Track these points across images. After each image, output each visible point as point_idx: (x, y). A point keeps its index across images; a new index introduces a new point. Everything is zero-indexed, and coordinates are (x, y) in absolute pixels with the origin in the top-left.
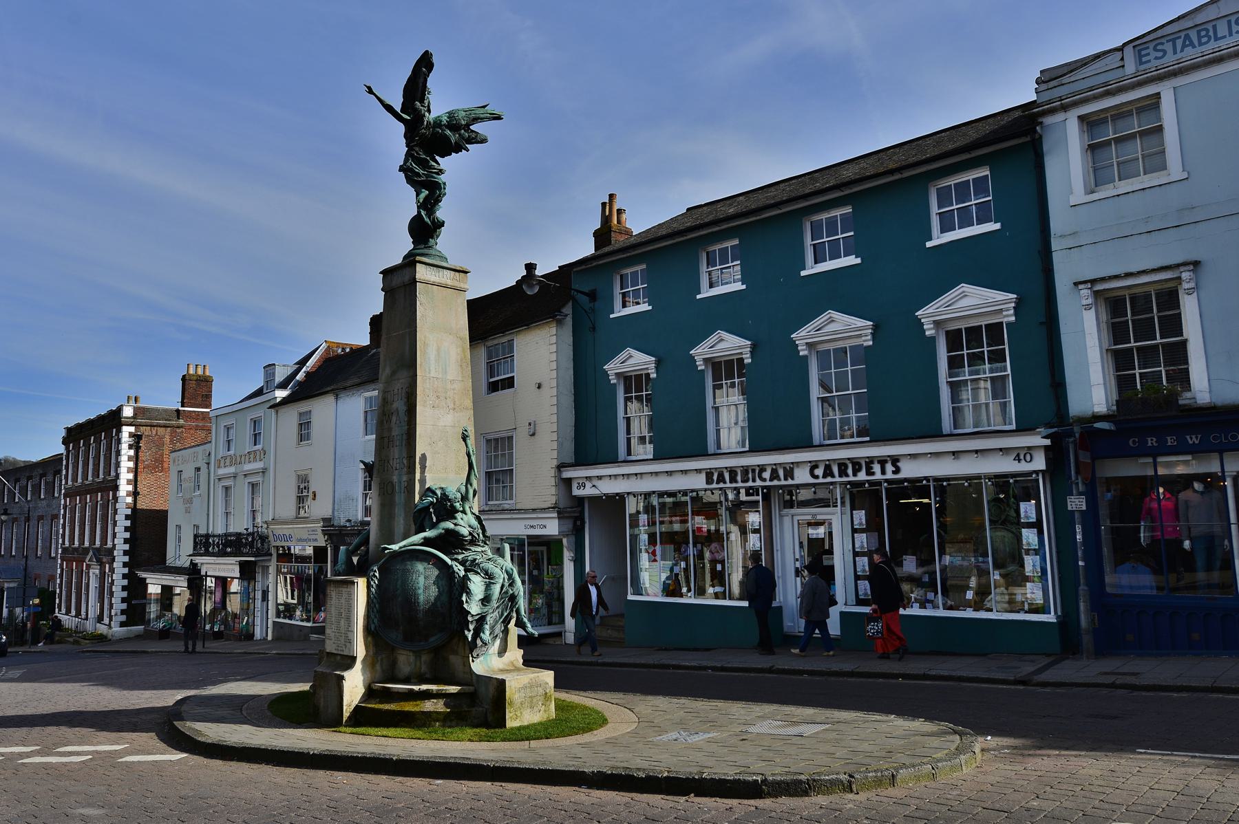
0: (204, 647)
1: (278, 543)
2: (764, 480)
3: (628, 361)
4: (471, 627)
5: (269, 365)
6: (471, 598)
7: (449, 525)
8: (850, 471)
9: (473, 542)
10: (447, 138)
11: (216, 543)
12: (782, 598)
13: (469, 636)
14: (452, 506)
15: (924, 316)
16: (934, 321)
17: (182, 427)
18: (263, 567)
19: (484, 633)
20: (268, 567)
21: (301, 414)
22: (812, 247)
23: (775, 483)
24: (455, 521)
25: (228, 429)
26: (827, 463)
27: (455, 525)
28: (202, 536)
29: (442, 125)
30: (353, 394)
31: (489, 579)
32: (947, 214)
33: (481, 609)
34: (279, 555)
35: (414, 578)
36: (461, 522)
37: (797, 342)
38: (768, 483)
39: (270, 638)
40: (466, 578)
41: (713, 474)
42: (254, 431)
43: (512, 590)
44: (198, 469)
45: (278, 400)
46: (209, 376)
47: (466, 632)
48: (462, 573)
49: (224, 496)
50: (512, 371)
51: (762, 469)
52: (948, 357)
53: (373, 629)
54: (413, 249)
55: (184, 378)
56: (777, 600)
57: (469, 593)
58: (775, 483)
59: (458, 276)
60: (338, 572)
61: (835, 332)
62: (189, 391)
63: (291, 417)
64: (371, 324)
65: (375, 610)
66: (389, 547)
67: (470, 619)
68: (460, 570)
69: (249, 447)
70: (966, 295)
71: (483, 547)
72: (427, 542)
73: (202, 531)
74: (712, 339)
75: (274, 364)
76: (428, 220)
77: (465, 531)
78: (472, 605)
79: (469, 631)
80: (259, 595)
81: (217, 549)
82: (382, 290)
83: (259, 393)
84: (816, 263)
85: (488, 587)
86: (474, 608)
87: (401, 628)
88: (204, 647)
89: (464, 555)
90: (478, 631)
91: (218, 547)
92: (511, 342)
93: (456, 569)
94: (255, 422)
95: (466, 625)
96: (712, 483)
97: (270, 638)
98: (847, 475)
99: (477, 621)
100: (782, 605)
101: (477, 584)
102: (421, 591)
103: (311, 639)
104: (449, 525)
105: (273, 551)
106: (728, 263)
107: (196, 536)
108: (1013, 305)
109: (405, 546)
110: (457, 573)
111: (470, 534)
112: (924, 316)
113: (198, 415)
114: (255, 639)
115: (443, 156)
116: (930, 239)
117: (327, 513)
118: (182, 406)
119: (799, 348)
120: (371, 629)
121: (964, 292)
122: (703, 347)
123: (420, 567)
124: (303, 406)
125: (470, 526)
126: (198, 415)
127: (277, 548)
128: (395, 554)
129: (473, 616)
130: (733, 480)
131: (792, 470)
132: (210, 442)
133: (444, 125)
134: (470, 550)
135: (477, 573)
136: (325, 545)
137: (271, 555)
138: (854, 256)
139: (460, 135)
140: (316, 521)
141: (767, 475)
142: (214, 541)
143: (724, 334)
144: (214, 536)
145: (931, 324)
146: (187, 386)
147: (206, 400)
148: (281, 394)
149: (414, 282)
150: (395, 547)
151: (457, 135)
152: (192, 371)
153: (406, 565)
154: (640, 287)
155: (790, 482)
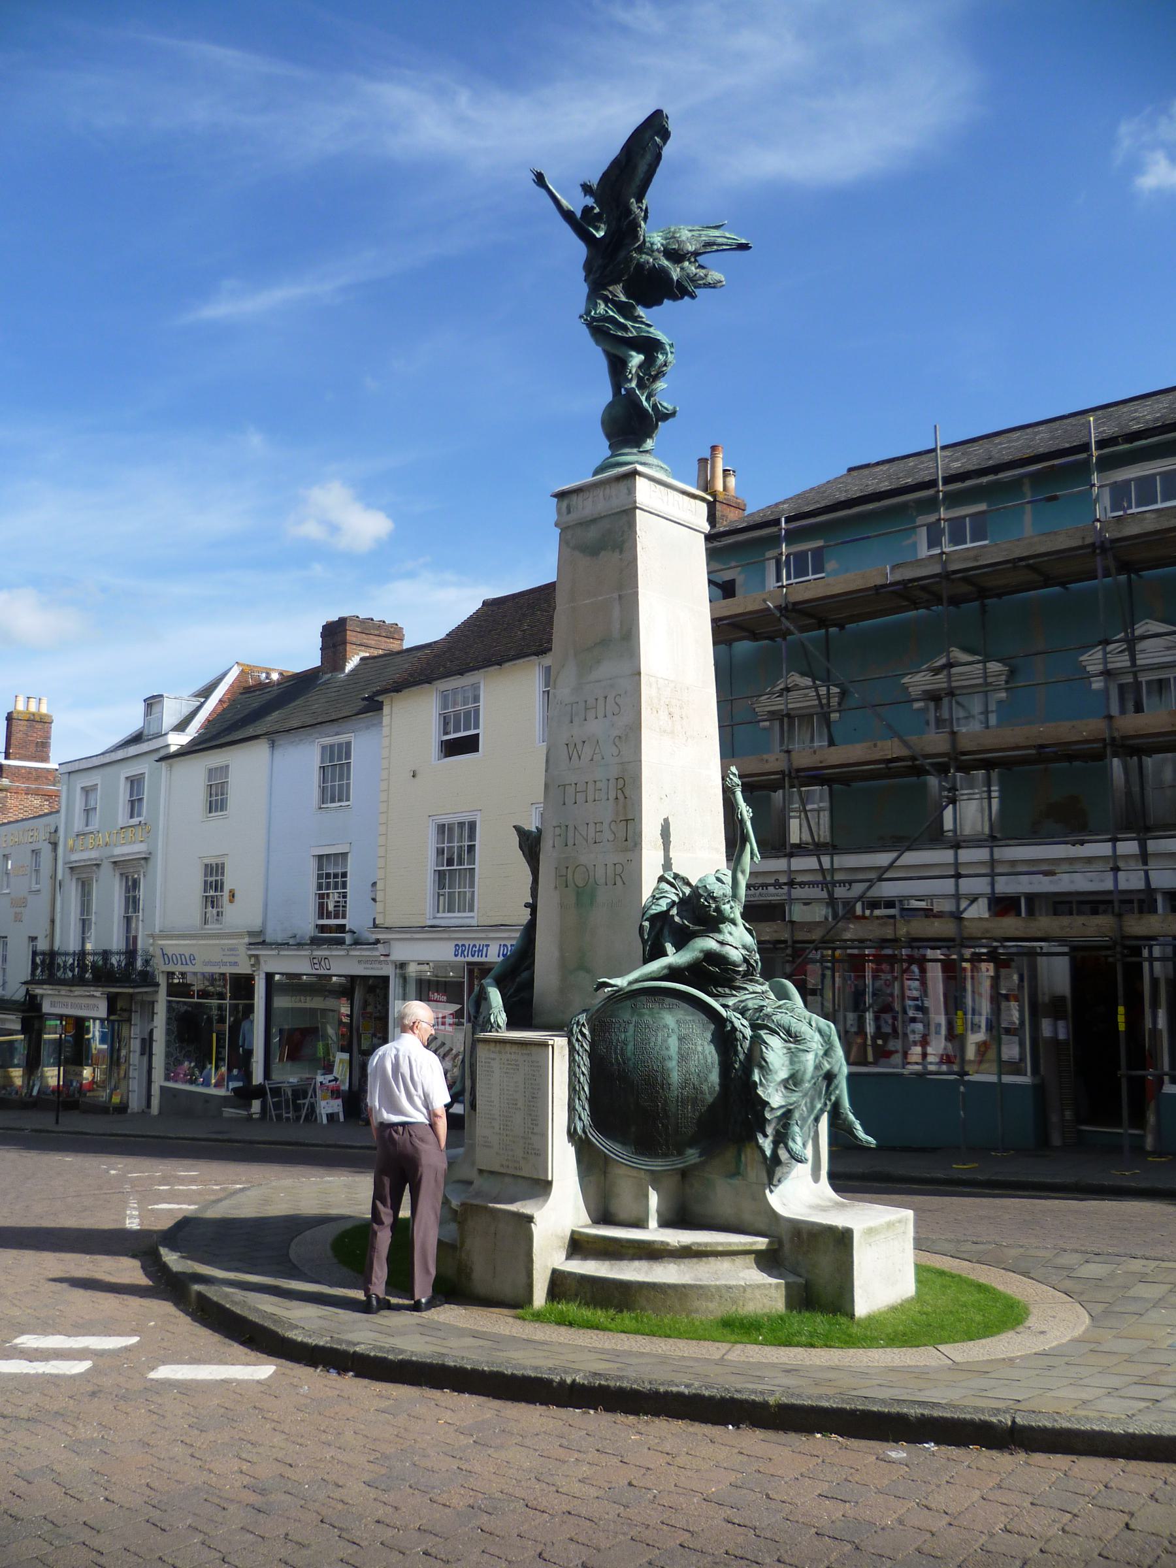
0: (57, 1122)
1: (170, 968)
4: (770, 1130)
5: (154, 697)
6: (769, 1077)
7: (710, 944)
9: (748, 975)
10: (663, 273)
11: (62, 970)
13: (767, 1144)
14: (718, 909)
15: (1091, 662)
17: (6, 790)
18: (143, 1003)
19: (794, 1140)
20: (153, 1003)
21: (211, 772)
24: (720, 937)
25: (87, 791)
27: (722, 943)
28: (43, 954)
29: (653, 251)
30: (301, 740)
31: (794, 1043)
33: (785, 1097)
34: (170, 986)
35: (660, 1039)
36: (729, 939)
39: (155, 1109)
40: (757, 1041)
42: (131, 795)
43: (829, 1063)
44: (36, 853)
45: (173, 749)
46: (46, 715)
47: (761, 1140)
48: (748, 1032)
49: (79, 895)
50: (477, 726)
53: (579, 1131)
54: (612, 456)
55: (10, 718)
57: (765, 1068)
59: (693, 505)
62: (17, 736)
63: (196, 771)
64: (323, 635)
65: (583, 1097)
66: (612, 981)
67: (768, 1116)
68: (742, 1024)
69: (122, 818)
71: (762, 984)
72: (674, 973)
73: (42, 945)
75: (161, 696)
76: (647, 405)
77: (735, 955)
78: (770, 1090)
79: (766, 1136)
80: (136, 1045)
81: (70, 974)
82: (556, 525)
83: (137, 739)
85: (793, 1056)
86: (775, 1098)
87: (633, 1129)
88: (57, 1122)
89: (738, 999)
90: (781, 1138)
91: (72, 970)
92: (476, 687)
93: (737, 1024)
94: (135, 783)
95: (760, 1124)
97: (155, 1109)
99: (779, 1118)
101: (776, 1051)
102: (672, 1064)
103: (225, 1115)
104: (710, 944)
105: (162, 980)
107: (35, 954)
109: (636, 981)
110: (741, 1032)
111: (746, 960)
112: (1091, 662)
113: (30, 773)
114: (129, 1111)
115: (648, 305)
117: (256, 924)
118: (7, 757)
120: (575, 1129)
123: (669, 1019)
124: (215, 759)
125: (744, 947)
126: (30, 773)
127: (170, 975)
128: (621, 997)
129: (772, 1109)
130: (339, 906)
132: (58, 812)
133: (658, 250)
134: (746, 989)
135: (773, 1032)
136: (249, 972)
137: (158, 985)
139: (682, 269)
140: (239, 935)
142: (65, 962)
144: (66, 954)
146: (14, 729)
147: (41, 750)
148: (176, 741)
149: (628, 513)
150: (621, 982)
151: (678, 269)
152: (21, 707)
153: (641, 1015)
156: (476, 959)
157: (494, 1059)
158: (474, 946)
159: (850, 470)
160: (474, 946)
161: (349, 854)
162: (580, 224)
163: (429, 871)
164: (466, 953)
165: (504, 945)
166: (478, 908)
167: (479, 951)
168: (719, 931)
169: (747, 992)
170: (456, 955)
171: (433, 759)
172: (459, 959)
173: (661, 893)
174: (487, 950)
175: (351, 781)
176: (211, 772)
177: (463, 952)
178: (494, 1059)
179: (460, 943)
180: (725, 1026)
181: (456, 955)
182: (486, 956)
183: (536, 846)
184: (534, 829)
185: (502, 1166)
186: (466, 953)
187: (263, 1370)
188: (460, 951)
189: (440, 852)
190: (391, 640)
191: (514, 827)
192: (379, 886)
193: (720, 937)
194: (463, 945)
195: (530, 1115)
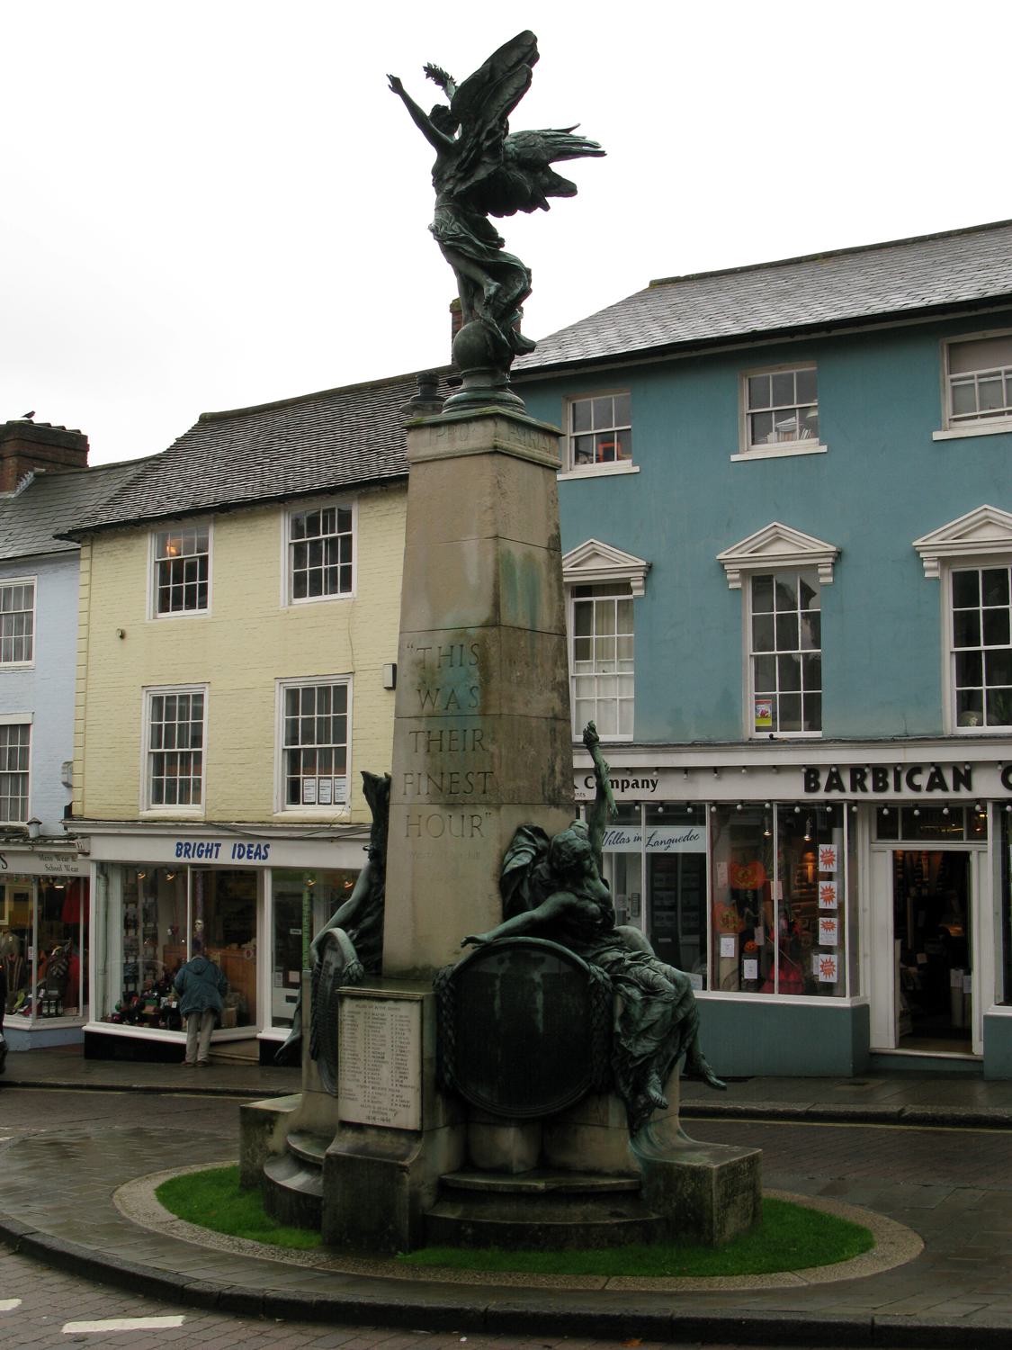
2: (917, 788)
3: (971, 535)
8: (869, 783)
12: (868, 994)
16: (939, 558)
22: (573, 441)
23: (938, 794)
24: (580, 892)
26: (834, 770)
32: (608, 435)
37: (922, 555)
38: (924, 795)
41: (817, 775)
51: (916, 769)
52: (955, 613)
56: (862, 994)
58: (938, 794)
60: (354, 978)
61: (998, 543)
70: (990, 522)
72: (533, 927)
74: (761, 534)
84: (753, 444)
96: (816, 789)
98: (864, 789)
100: (868, 1001)
106: (768, 406)
108: (642, 574)
116: (737, 452)
119: (925, 564)
121: (987, 517)
122: (740, 551)
131: (969, 773)
134: (604, 941)
138: (631, 461)
141: (922, 780)
143: (600, 546)
145: (934, 561)
154: (614, 429)
155: (964, 794)
156: (204, 860)
157: (359, 1013)
158: (202, 845)
159: (657, 285)
160: (202, 845)
161: (32, 727)
162: (433, 125)
163: (142, 752)
164: (191, 853)
165: (240, 845)
166: (207, 800)
167: (207, 851)
168: (582, 887)
169: (604, 944)
170: (178, 856)
171: (147, 618)
172: (183, 860)
173: (521, 847)
174: (218, 850)
175: (34, 635)
176: (188, 792)
177: (187, 852)
178: (359, 1013)
179: (184, 841)
180: (588, 980)
181: (178, 856)
182: (216, 857)
183: (385, 792)
184: (383, 776)
185: (369, 1118)
186: (191, 853)
187: (174, 1321)
188: (183, 851)
189: (156, 730)
190: (73, 452)
191: (363, 773)
192: (77, 767)
193: (580, 892)
194: (187, 844)
195: (399, 1068)
